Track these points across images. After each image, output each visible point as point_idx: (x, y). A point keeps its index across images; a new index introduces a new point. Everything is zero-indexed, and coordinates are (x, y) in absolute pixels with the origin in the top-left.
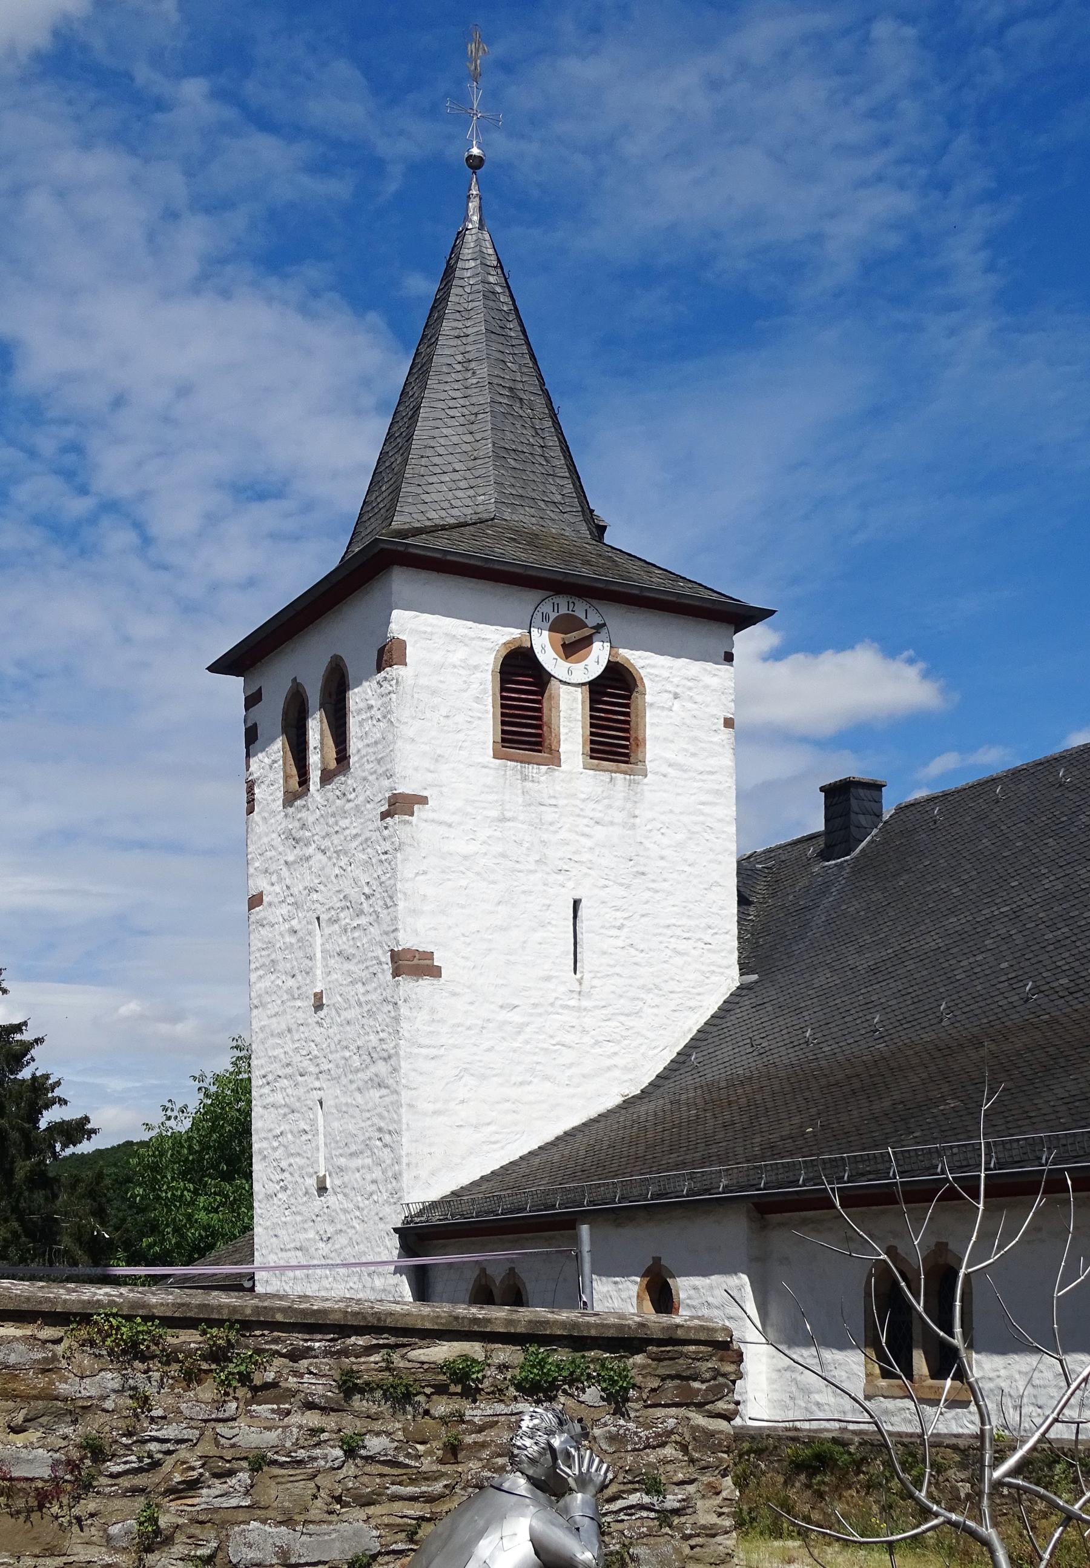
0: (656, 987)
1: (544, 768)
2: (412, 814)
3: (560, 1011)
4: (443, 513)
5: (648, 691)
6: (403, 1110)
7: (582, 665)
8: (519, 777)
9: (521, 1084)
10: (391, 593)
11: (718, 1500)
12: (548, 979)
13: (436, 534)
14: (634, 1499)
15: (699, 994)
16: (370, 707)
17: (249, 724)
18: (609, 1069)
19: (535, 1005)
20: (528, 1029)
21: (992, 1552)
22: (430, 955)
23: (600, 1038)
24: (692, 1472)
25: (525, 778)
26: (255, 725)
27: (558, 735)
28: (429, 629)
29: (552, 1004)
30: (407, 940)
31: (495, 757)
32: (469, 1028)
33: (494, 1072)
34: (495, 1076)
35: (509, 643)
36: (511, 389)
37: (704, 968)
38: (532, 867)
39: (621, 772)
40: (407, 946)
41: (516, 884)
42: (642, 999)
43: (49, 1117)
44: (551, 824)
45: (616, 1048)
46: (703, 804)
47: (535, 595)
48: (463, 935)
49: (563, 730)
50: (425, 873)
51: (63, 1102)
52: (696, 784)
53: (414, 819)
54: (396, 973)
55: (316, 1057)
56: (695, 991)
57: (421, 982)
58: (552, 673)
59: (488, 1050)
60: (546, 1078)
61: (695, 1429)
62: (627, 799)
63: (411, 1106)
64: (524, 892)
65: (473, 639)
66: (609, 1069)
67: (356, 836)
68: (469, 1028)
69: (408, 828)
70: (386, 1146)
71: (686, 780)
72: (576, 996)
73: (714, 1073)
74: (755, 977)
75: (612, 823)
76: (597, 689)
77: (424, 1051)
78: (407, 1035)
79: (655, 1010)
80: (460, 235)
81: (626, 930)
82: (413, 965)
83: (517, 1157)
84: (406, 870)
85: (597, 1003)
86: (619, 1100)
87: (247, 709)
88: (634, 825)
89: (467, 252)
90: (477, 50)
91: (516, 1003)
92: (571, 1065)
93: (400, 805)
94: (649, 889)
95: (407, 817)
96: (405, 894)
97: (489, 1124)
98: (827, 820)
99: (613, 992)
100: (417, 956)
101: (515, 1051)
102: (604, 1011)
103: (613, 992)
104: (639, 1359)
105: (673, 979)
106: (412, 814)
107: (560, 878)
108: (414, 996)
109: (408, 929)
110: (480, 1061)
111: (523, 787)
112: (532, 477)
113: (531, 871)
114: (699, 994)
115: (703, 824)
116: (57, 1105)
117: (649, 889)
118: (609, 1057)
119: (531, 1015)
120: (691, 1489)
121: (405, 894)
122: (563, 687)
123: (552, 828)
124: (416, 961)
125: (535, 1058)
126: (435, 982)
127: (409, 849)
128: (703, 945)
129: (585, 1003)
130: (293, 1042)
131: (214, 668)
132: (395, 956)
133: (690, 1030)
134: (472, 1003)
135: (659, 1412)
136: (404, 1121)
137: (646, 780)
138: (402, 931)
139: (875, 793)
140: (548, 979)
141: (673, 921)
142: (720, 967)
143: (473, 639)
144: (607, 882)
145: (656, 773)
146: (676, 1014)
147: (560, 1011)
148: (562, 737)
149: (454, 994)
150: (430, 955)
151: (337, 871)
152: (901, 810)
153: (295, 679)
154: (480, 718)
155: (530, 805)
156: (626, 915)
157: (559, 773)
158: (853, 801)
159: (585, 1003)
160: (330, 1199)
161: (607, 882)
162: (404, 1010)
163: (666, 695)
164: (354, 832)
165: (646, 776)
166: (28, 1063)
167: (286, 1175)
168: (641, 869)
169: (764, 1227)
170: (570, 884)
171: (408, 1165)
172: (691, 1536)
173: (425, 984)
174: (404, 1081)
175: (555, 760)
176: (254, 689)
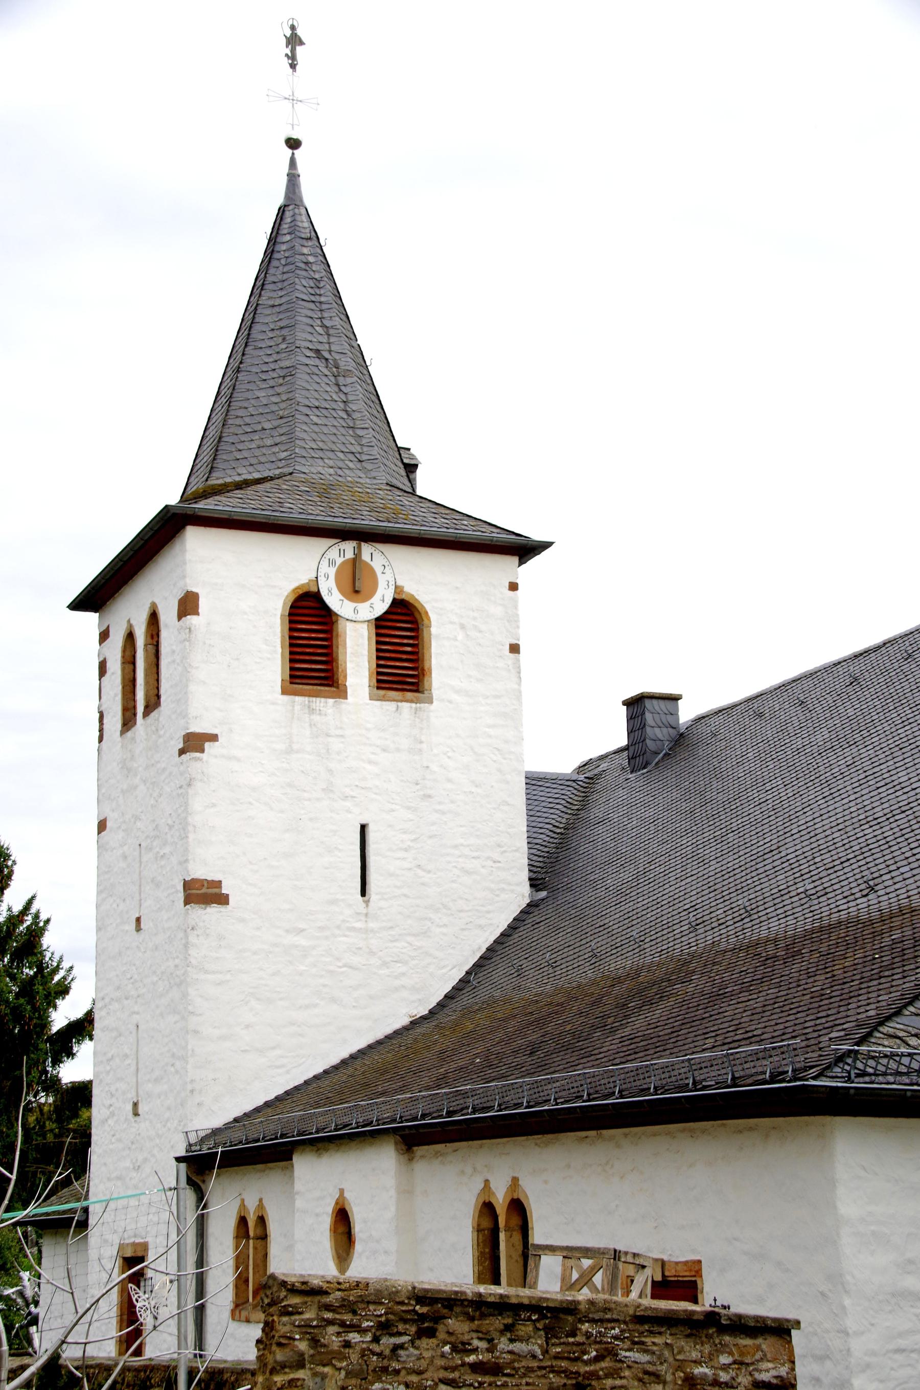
0: (445, 906)
2: (202, 751)
3: (347, 933)
5: (433, 623)
7: (367, 604)
8: (307, 711)
10: (185, 551)
12: (334, 902)
15: (488, 912)
16: (174, 652)
17: (102, 659)
18: (397, 989)
19: (321, 929)
22: (219, 884)
23: (388, 959)
25: (312, 711)
26: (105, 659)
27: (345, 671)
29: (338, 927)
30: (200, 872)
32: (255, 953)
34: (281, 999)
35: (297, 588)
37: (492, 886)
39: (407, 701)
41: (302, 812)
42: (430, 919)
44: (339, 753)
45: (404, 969)
47: (325, 543)
48: (251, 863)
49: (349, 665)
50: (214, 805)
53: (204, 756)
54: (187, 902)
55: (136, 981)
56: (484, 909)
58: (339, 613)
59: (273, 974)
60: (333, 1000)
64: (311, 819)
66: (397, 989)
67: (164, 769)
68: (255, 953)
69: (198, 765)
70: (177, 1072)
72: (363, 918)
73: (538, 984)
75: (398, 750)
76: (381, 624)
77: (210, 977)
79: (444, 930)
82: (204, 894)
83: (301, 1081)
84: (197, 804)
86: (406, 1021)
87: (100, 644)
88: (420, 750)
93: (194, 743)
94: (436, 811)
95: (198, 755)
97: (274, 1048)
98: (630, 732)
99: (400, 913)
100: (206, 884)
101: (301, 974)
103: (400, 913)
105: (461, 898)
106: (202, 751)
107: (348, 804)
108: (201, 924)
110: (266, 985)
113: (318, 799)
114: (488, 912)
117: (436, 811)
118: (396, 978)
121: (194, 826)
122: (348, 623)
124: (204, 890)
128: (491, 863)
129: (372, 925)
132: (187, 885)
134: (258, 929)
136: (190, 1047)
138: (191, 862)
139: (669, 704)
140: (334, 902)
141: (462, 841)
142: (510, 884)
144: (394, 807)
145: (442, 700)
147: (347, 933)
148: (348, 672)
149: (242, 920)
150: (219, 884)
151: (152, 802)
153: (129, 621)
154: (269, 659)
155: (317, 737)
156: (413, 837)
158: (648, 716)
159: (372, 925)
161: (394, 807)
164: (163, 765)
165: (432, 702)
167: (114, 1100)
168: (429, 792)
169: (411, 1160)
173: (213, 910)
176: (104, 628)
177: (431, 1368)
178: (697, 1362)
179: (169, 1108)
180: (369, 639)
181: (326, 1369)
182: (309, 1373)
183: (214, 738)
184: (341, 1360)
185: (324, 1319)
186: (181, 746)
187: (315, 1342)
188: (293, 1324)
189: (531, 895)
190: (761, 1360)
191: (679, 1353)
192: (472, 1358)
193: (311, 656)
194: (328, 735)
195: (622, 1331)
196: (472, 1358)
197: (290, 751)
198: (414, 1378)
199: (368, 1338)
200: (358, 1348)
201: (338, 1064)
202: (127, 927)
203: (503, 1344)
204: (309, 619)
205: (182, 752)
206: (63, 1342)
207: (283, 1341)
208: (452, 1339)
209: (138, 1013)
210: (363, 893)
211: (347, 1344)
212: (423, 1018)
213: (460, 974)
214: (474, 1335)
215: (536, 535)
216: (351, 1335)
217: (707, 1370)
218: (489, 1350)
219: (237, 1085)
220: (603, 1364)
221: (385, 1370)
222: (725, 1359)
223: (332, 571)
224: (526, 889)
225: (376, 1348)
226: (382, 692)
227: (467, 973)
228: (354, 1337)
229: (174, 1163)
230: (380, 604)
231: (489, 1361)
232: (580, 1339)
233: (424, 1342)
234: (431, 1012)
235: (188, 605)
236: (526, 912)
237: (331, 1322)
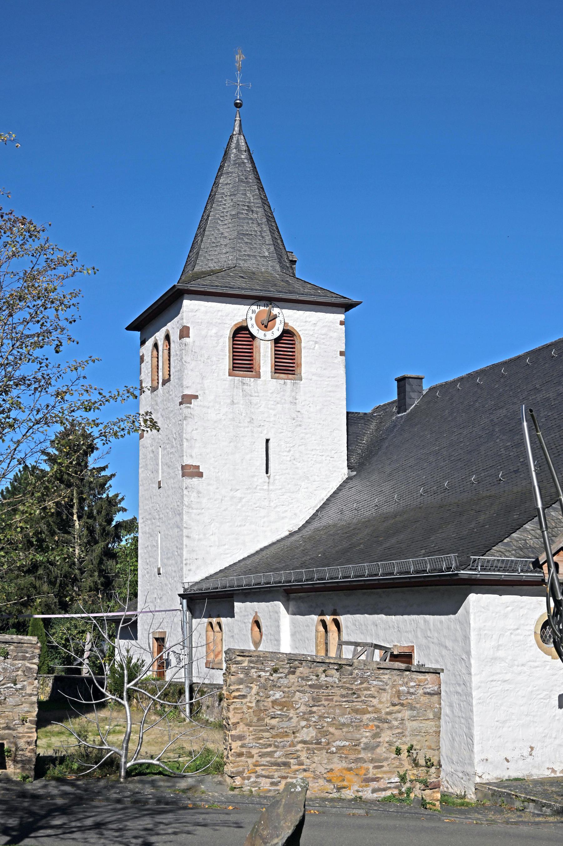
1: (252, 379)
2: (191, 403)
4: (215, 265)
6: (185, 538)
7: (271, 332)
9: (240, 526)
11: (32, 687)
13: (205, 278)
14: (9, 685)
20: (244, 500)
21: (125, 708)
24: (25, 678)
28: (200, 321)
30: (188, 461)
31: (229, 375)
33: (227, 521)
34: (228, 522)
36: (248, 206)
38: (246, 424)
40: (187, 463)
43: (118, 518)
46: (330, 392)
50: (196, 429)
51: (124, 510)
52: (326, 383)
53: (192, 406)
54: (183, 476)
57: (194, 479)
59: (225, 510)
61: (26, 667)
62: (292, 391)
63: (188, 537)
65: (220, 324)
67: (172, 411)
71: (321, 381)
74: (355, 473)
78: (186, 503)
80: (231, 137)
81: (292, 452)
83: (237, 561)
85: (277, 487)
86: (287, 533)
89: (233, 145)
90: (240, 58)
91: (238, 488)
92: (264, 517)
93: (187, 399)
95: (189, 405)
96: (187, 439)
102: (280, 491)
104: (12, 647)
106: (191, 403)
107: (260, 429)
109: (188, 455)
111: (243, 388)
112: (255, 246)
115: (329, 401)
116: (121, 512)
119: (245, 494)
120: (25, 683)
122: (261, 341)
123: (256, 407)
125: (247, 514)
126: (200, 479)
127: (190, 419)
130: (152, 503)
131: (128, 328)
132: (183, 467)
133: (323, 499)
135: (17, 662)
136: (184, 543)
137: (302, 382)
143: (220, 324)
146: (316, 492)
152: (432, 389)
156: (292, 445)
157: (259, 381)
158: (407, 386)
160: (162, 578)
162: (185, 492)
163: (311, 343)
164: (172, 409)
166: (108, 488)
170: (265, 432)
171: (186, 564)
172: (24, 696)
173: (195, 481)
174: (185, 525)
175: (258, 376)
177: (293, 686)
178: (402, 685)
179: (175, 572)
180: (271, 349)
181: (251, 685)
182: (244, 686)
183: (196, 397)
184: (257, 682)
185: (250, 666)
186: (180, 400)
187: (247, 674)
188: (238, 668)
189: (348, 474)
190: (427, 684)
191: (394, 682)
192: (310, 683)
193: (242, 358)
194: (251, 396)
195: (371, 673)
196: (310, 683)
197: (233, 403)
198: (286, 689)
199: (268, 674)
200: (264, 678)
201: (255, 553)
202: (154, 486)
203: (323, 677)
204: (241, 333)
205: (181, 403)
206: (148, 670)
207: (234, 674)
208: (302, 675)
209: (159, 526)
210: (267, 472)
211: (259, 676)
212: (295, 532)
213: (313, 512)
214: (311, 674)
215: (355, 299)
216: (261, 673)
217: (405, 688)
218: (316, 680)
219: (206, 563)
220: (363, 686)
221: (275, 686)
222: (412, 684)
223: (254, 316)
224: (345, 470)
225: (272, 678)
226: (277, 375)
227: (317, 511)
228: (262, 674)
229: (179, 598)
230: (276, 332)
231: (317, 684)
232: (354, 675)
233: (291, 676)
234: (299, 529)
235: (184, 332)
236: (345, 482)
237: (253, 668)
